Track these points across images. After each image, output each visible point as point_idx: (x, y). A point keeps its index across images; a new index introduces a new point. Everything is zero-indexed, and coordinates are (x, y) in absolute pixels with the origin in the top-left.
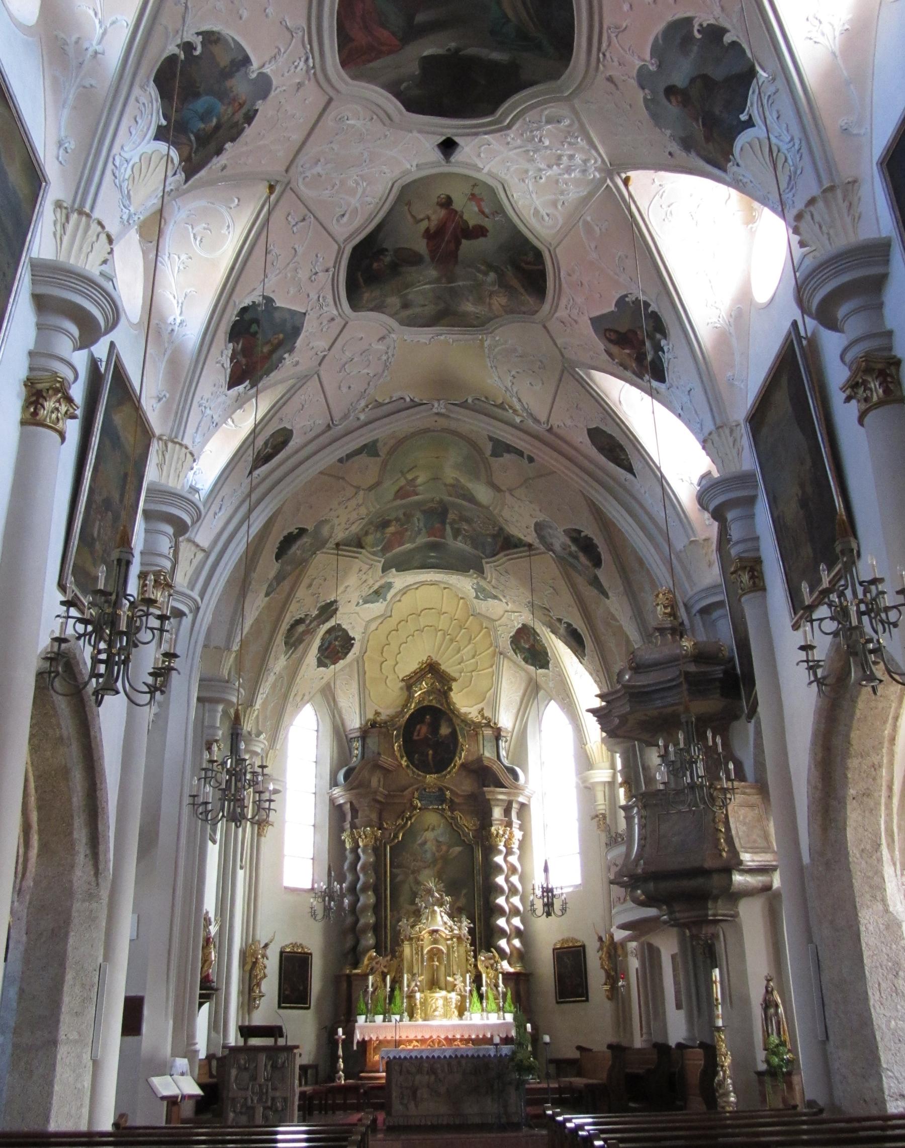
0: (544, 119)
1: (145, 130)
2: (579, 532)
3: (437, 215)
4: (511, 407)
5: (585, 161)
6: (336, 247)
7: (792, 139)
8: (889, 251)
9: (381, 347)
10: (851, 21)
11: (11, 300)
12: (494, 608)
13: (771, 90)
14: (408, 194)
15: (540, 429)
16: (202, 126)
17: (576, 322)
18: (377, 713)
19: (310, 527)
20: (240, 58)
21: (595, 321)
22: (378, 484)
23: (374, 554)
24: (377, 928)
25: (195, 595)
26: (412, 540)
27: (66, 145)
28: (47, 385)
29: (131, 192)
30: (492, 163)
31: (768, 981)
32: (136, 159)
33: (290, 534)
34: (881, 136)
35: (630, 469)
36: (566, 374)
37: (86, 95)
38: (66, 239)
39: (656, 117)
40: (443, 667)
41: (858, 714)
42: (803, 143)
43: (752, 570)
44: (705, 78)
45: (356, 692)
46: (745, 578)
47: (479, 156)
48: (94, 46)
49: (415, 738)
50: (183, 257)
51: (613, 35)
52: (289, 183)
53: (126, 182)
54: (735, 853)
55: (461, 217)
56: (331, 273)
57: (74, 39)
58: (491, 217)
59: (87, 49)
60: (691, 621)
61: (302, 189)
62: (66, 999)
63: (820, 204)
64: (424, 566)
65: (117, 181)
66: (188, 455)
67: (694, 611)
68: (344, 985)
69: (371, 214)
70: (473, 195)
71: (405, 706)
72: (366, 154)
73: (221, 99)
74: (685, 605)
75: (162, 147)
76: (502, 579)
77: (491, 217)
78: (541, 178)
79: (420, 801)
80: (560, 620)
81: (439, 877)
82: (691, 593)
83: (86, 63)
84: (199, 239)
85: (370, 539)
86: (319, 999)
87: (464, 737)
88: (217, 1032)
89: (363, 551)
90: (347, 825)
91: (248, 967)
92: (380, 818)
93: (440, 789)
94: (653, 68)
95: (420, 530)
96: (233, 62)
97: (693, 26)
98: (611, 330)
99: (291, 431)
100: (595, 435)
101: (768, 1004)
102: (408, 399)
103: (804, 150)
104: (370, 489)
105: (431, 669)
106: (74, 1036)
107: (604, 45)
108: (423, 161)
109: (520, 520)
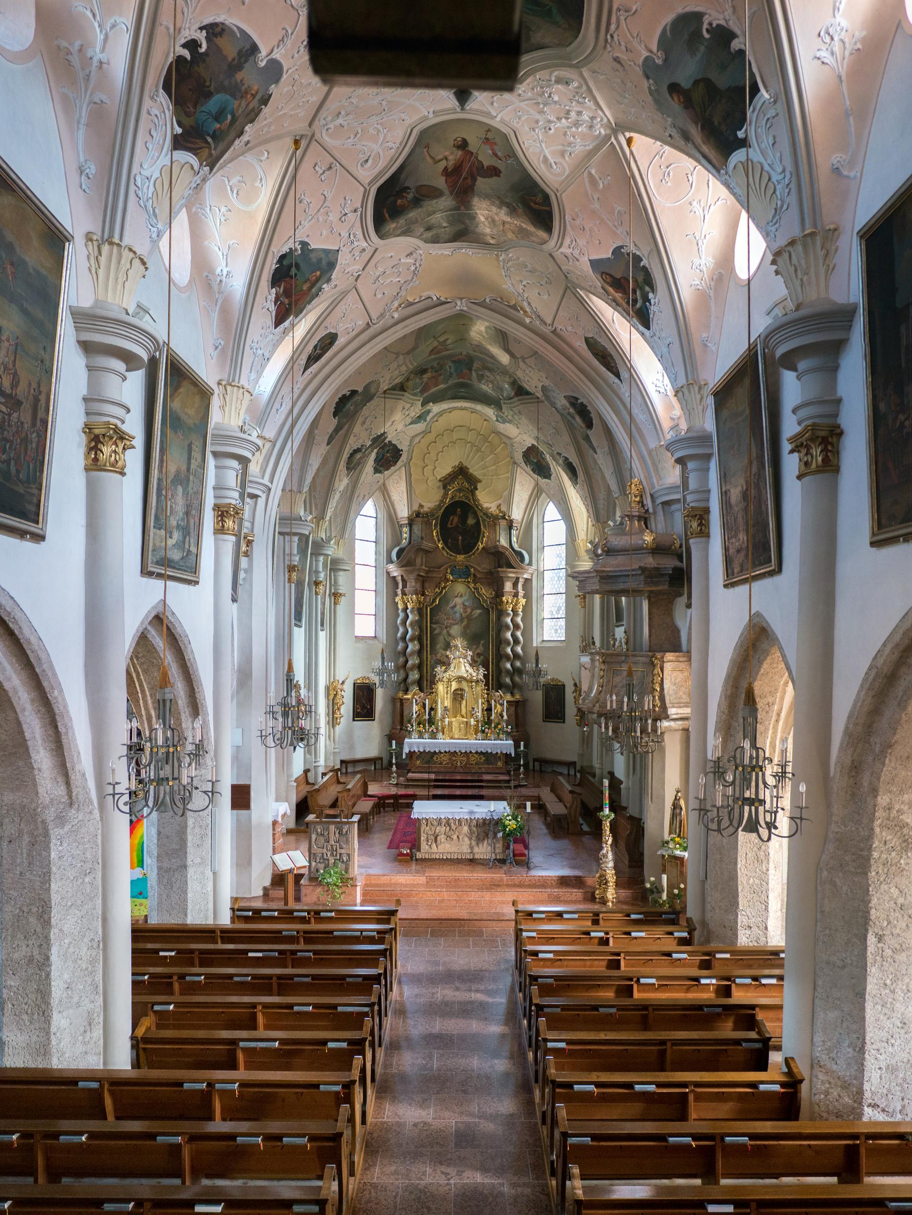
0: (553, 79)
1: (161, 142)
2: (577, 399)
3: (454, 156)
4: (522, 309)
5: (592, 118)
6: (362, 189)
7: (784, 171)
8: (853, 316)
9: (410, 260)
10: (863, 40)
11: (54, 380)
12: (510, 430)
13: (771, 113)
14: (426, 138)
15: (547, 330)
16: (217, 126)
17: (578, 260)
18: (421, 506)
19: (360, 389)
20: (248, 46)
21: (595, 264)
22: (414, 349)
23: (415, 395)
24: (420, 667)
25: (266, 481)
26: (445, 381)
27: (88, 171)
28: (103, 431)
29: (156, 210)
30: (504, 112)
31: (678, 792)
32: (156, 174)
33: (344, 396)
34: (870, 199)
35: (618, 376)
36: (568, 291)
37: (98, 112)
38: (101, 272)
39: (659, 104)
40: (471, 471)
41: (762, 671)
42: (794, 179)
43: (701, 518)
44: (707, 83)
45: (404, 489)
46: (695, 524)
47: (492, 104)
48: (99, 56)
49: (449, 526)
50: (223, 209)
51: (622, 18)
52: (313, 135)
53: (151, 201)
54: (664, 708)
55: (477, 158)
56: (359, 213)
57: (77, 44)
58: (504, 159)
59: (91, 58)
60: (654, 507)
61: (327, 139)
62: (190, 837)
63: (799, 248)
64: (455, 397)
65: (141, 202)
66: (246, 393)
67: (659, 501)
68: (398, 704)
69: (392, 158)
70: (487, 139)
71: (442, 501)
72: (384, 103)
73: (233, 95)
74: (652, 496)
75: (184, 156)
76: (516, 417)
77: (504, 159)
78: (550, 129)
79: (452, 575)
80: (559, 454)
81: (464, 635)
82: (657, 488)
83: (93, 74)
84: (235, 192)
85: (410, 383)
86: (381, 714)
87: (485, 527)
88: (311, 754)
89: (406, 394)
90: (399, 591)
91: (331, 697)
92: (423, 587)
93: (466, 567)
94: (659, 62)
95: (451, 374)
96: (240, 53)
97: (702, 23)
98: (607, 274)
99: (336, 335)
100: (590, 343)
101: (676, 806)
102: (435, 298)
103: (793, 186)
104: (408, 353)
105: (461, 472)
106: (198, 860)
107: (613, 27)
108: (438, 108)
109: (533, 380)
